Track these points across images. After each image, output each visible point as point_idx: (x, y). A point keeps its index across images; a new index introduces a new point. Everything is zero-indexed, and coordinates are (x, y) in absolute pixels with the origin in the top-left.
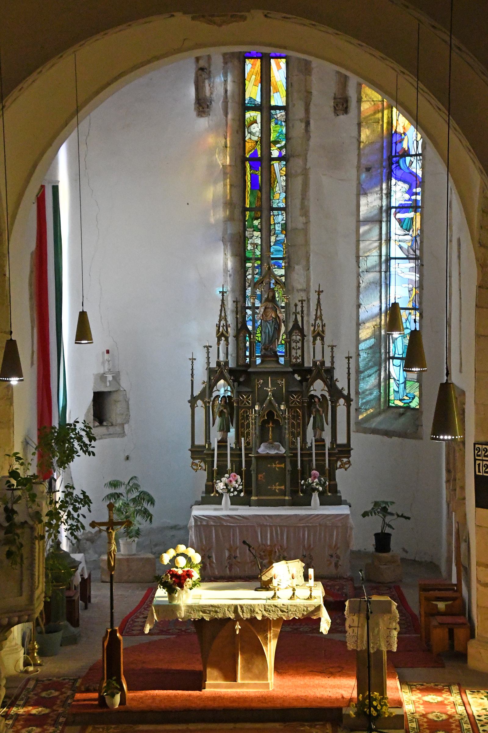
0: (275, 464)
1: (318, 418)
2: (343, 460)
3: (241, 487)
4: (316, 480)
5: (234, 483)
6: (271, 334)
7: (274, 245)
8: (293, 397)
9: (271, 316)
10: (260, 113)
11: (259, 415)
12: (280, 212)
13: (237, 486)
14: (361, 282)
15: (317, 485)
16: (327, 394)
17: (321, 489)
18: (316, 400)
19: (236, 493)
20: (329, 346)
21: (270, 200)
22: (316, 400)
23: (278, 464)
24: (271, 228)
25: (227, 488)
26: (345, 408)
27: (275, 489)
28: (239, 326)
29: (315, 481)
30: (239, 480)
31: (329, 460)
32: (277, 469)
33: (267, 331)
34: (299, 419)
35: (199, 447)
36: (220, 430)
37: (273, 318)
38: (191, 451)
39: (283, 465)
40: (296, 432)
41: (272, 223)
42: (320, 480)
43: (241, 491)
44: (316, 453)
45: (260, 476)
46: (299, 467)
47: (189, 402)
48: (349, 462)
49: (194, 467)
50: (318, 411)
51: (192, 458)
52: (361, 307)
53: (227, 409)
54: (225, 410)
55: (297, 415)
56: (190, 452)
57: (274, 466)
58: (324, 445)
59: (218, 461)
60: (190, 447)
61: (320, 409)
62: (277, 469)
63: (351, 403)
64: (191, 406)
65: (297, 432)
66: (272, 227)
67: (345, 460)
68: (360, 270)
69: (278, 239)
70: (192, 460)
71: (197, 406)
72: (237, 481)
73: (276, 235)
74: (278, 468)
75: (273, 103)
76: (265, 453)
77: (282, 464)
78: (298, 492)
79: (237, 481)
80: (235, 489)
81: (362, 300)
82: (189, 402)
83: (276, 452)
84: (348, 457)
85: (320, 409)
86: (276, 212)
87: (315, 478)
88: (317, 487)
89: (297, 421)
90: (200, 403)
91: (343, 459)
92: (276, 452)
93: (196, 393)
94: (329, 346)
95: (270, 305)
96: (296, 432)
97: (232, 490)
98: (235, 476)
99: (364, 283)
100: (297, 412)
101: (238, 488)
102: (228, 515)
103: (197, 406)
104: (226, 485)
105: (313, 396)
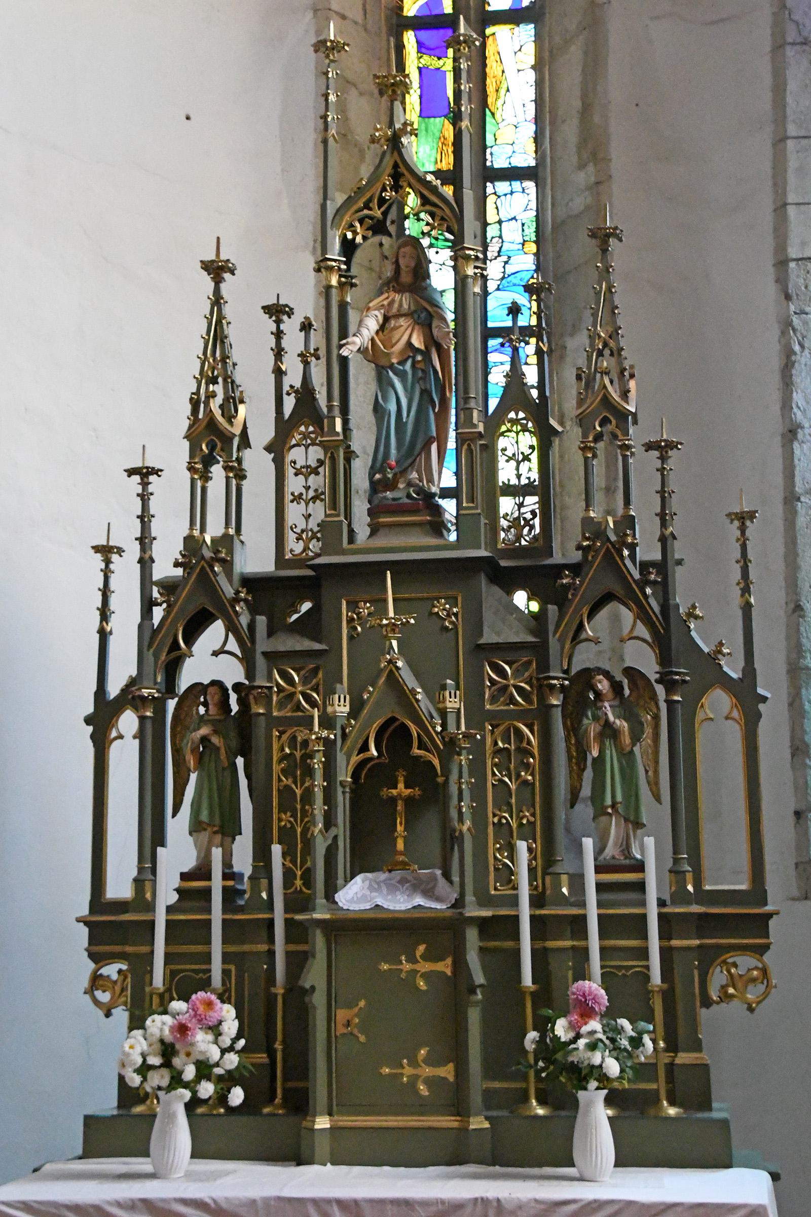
0: (412, 960)
1: (611, 756)
2: (735, 965)
3: (232, 1060)
4: (595, 1025)
5: (203, 1042)
6: (409, 420)
7: (498, 289)
8: (501, 673)
9: (409, 344)
10: (534, 184)
11: (344, 736)
12: (516, 185)
13: (214, 1053)
14: (797, 348)
15: (592, 1047)
16: (650, 667)
17: (613, 1067)
18: (603, 685)
19: (207, 1089)
20: (649, 447)
21: (485, 147)
22: (603, 685)
23: (426, 957)
24: (489, 236)
25: (167, 1064)
26: (734, 733)
27: (414, 1079)
28: (289, 403)
29: (585, 1029)
30: (231, 1027)
31: (666, 953)
32: (422, 984)
33: (392, 407)
34: (527, 766)
35: (120, 906)
36: (196, 827)
37: (418, 350)
38: (86, 923)
39: (449, 961)
40: (514, 825)
41: (491, 217)
42: (613, 1032)
43: (228, 1080)
44: (602, 919)
45: (342, 1015)
46: (527, 979)
47: (88, 720)
48: (764, 971)
49: (99, 994)
50: (609, 732)
51: (92, 956)
52: (800, 435)
53: (225, 737)
54: (215, 740)
55: (519, 749)
56: (85, 931)
57: (407, 966)
58: (641, 887)
59: (169, 958)
60: (85, 911)
61: (622, 724)
62: (422, 984)
63: (761, 707)
64: (92, 737)
65: (521, 825)
66: (492, 231)
67: (745, 963)
68: (792, 308)
69: (510, 269)
70: (92, 966)
71: (121, 737)
72: (215, 1029)
73: (505, 258)
74: (425, 976)
75: (527, 31)
76: (368, 906)
77: (442, 959)
78: (525, 1099)
79: (215, 1029)
80: (204, 1069)
81: (804, 412)
82: (88, 720)
83: (419, 900)
84: (762, 950)
85: (622, 724)
86: (502, 187)
87: (587, 1013)
88: (596, 1058)
89: (518, 776)
90: (128, 721)
91: (738, 960)
92: (419, 900)
93: (114, 689)
94: (649, 447)
95: (404, 301)
96: (514, 825)
97: (190, 1072)
98: (209, 1004)
99: (807, 352)
100: (519, 734)
101: (217, 1065)
102: (144, 1201)
103: (121, 737)
104: (168, 1051)
105: (586, 676)
